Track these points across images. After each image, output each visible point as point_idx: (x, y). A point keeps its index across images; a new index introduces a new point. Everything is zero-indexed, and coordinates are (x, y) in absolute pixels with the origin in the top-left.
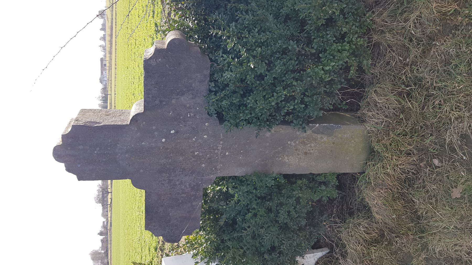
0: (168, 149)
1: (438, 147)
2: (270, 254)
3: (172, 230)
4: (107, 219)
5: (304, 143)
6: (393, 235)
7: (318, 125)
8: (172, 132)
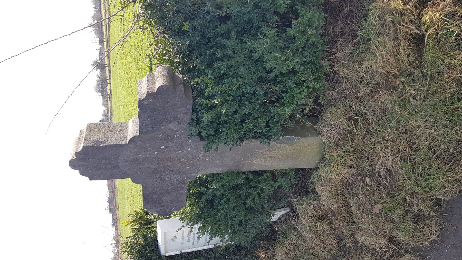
3: (164, 208)
4: (108, 108)
5: (269, 150)
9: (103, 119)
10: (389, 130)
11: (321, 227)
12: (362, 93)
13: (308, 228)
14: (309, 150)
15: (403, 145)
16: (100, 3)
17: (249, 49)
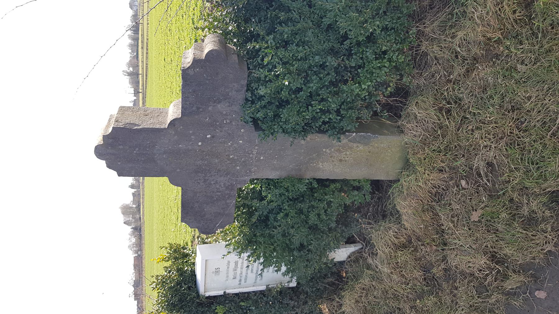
0: (204, 151)
1: (467, 169)
2: (300, 251)
3: (206, 223)
5: (339, 151)
6: (420, 243)
7: (355, 134)
8: (208, 136)
9: (133, 185)
10: (491, 109)
11: (403, 257)
12: (456, 74)
13: (386, 261)
14: (389, 154)
15: (508, 125)
16: (138, 48)
17: (318, 14)
